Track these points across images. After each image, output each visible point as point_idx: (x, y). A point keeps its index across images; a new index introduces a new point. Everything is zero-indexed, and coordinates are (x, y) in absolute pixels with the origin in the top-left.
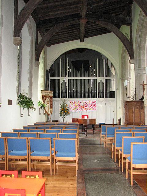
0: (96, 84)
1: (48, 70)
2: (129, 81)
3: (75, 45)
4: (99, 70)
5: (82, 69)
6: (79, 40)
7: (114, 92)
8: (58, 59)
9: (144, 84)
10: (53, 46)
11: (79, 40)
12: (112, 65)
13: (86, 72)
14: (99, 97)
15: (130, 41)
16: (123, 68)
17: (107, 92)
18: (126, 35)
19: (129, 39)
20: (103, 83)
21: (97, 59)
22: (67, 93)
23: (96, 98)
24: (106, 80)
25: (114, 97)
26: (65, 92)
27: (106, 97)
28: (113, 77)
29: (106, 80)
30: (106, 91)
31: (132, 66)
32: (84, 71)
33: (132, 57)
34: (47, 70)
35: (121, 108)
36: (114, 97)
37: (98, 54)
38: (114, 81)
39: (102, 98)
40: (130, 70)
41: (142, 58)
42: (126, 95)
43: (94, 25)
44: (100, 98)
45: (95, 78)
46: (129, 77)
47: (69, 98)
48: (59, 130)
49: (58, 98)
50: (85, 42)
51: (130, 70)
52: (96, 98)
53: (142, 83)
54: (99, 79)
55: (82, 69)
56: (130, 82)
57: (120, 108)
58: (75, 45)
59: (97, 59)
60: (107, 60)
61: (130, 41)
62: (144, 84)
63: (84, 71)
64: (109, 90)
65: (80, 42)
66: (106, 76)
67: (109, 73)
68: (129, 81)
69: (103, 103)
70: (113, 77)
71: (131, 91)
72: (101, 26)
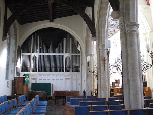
0: (63, 60)
1: (20, 47)
2: (92, 57)
3: (45, 24)
4: (66, 47)
5: (51, 46)
6: (49, 20)
7: (79, 67)
8: (30, 36)
9: (105, 59)
10: (25, 25)
11: (49, 20)
12: (78, 43)
13: (55, 49)
14: (67, 71)
15: (92, 20)
16: (88, 46)
17: (73, 67)
18: (89, 16)
19: (8, 10)
20: (69, 58)
21: (71, 38)
22: (37, 67)
23: (36, 72)
24: (72, 56)
25: (79, 71)
26: (35, 67)
27: (72, 71)
28: (79, 53)
29: (72, 56)
30: (72, 66)
31: (95, 43)
32: (53, 48)
33: (94, 34)
34: (19, 46)
35: (86, 81)
36: (79, 71)
37: (65, 34)
38: (79, 57)
39: (69, 72)
40: (93, 47)
41: (102, 36)
42: (89, 69)
43: (62, 7)
44: (67, 72)
45: (29, 54)
46: (92, 53)
47: (32, 72)
48: (92, 99)
49: (62, 72)
50: (54, 22)
51: (93, 47)
52: (36, 72)
53: (103, 59)
54: (66, 55)
55: (51, 46)
56: (94, 58)
57: (85, 81)
58: (45, 24)
59: (71, 38)
60: (73, 38)
61: (92, 20)
62: (105, 59)
63: (53, 48)
64: (75, 65)
65: (50, 21)
66: (72, 53)
67: (75, 50)
68: (93, 57)
69: (70, 77)
70: (79, 53)
71: (94, 66)
72: (69, 8)
